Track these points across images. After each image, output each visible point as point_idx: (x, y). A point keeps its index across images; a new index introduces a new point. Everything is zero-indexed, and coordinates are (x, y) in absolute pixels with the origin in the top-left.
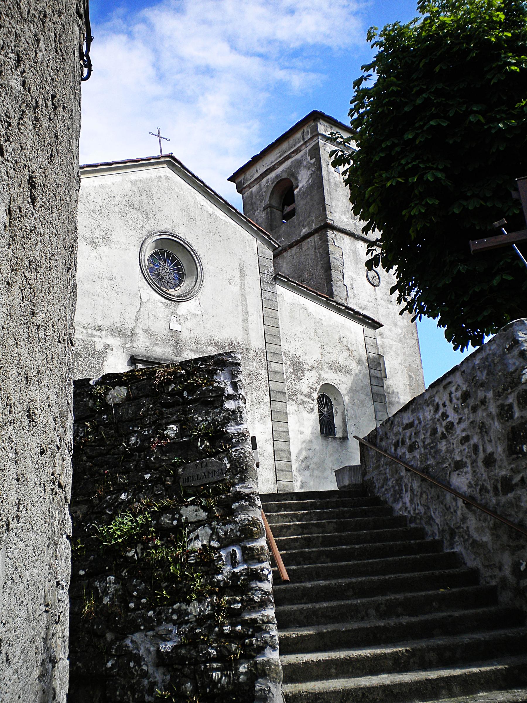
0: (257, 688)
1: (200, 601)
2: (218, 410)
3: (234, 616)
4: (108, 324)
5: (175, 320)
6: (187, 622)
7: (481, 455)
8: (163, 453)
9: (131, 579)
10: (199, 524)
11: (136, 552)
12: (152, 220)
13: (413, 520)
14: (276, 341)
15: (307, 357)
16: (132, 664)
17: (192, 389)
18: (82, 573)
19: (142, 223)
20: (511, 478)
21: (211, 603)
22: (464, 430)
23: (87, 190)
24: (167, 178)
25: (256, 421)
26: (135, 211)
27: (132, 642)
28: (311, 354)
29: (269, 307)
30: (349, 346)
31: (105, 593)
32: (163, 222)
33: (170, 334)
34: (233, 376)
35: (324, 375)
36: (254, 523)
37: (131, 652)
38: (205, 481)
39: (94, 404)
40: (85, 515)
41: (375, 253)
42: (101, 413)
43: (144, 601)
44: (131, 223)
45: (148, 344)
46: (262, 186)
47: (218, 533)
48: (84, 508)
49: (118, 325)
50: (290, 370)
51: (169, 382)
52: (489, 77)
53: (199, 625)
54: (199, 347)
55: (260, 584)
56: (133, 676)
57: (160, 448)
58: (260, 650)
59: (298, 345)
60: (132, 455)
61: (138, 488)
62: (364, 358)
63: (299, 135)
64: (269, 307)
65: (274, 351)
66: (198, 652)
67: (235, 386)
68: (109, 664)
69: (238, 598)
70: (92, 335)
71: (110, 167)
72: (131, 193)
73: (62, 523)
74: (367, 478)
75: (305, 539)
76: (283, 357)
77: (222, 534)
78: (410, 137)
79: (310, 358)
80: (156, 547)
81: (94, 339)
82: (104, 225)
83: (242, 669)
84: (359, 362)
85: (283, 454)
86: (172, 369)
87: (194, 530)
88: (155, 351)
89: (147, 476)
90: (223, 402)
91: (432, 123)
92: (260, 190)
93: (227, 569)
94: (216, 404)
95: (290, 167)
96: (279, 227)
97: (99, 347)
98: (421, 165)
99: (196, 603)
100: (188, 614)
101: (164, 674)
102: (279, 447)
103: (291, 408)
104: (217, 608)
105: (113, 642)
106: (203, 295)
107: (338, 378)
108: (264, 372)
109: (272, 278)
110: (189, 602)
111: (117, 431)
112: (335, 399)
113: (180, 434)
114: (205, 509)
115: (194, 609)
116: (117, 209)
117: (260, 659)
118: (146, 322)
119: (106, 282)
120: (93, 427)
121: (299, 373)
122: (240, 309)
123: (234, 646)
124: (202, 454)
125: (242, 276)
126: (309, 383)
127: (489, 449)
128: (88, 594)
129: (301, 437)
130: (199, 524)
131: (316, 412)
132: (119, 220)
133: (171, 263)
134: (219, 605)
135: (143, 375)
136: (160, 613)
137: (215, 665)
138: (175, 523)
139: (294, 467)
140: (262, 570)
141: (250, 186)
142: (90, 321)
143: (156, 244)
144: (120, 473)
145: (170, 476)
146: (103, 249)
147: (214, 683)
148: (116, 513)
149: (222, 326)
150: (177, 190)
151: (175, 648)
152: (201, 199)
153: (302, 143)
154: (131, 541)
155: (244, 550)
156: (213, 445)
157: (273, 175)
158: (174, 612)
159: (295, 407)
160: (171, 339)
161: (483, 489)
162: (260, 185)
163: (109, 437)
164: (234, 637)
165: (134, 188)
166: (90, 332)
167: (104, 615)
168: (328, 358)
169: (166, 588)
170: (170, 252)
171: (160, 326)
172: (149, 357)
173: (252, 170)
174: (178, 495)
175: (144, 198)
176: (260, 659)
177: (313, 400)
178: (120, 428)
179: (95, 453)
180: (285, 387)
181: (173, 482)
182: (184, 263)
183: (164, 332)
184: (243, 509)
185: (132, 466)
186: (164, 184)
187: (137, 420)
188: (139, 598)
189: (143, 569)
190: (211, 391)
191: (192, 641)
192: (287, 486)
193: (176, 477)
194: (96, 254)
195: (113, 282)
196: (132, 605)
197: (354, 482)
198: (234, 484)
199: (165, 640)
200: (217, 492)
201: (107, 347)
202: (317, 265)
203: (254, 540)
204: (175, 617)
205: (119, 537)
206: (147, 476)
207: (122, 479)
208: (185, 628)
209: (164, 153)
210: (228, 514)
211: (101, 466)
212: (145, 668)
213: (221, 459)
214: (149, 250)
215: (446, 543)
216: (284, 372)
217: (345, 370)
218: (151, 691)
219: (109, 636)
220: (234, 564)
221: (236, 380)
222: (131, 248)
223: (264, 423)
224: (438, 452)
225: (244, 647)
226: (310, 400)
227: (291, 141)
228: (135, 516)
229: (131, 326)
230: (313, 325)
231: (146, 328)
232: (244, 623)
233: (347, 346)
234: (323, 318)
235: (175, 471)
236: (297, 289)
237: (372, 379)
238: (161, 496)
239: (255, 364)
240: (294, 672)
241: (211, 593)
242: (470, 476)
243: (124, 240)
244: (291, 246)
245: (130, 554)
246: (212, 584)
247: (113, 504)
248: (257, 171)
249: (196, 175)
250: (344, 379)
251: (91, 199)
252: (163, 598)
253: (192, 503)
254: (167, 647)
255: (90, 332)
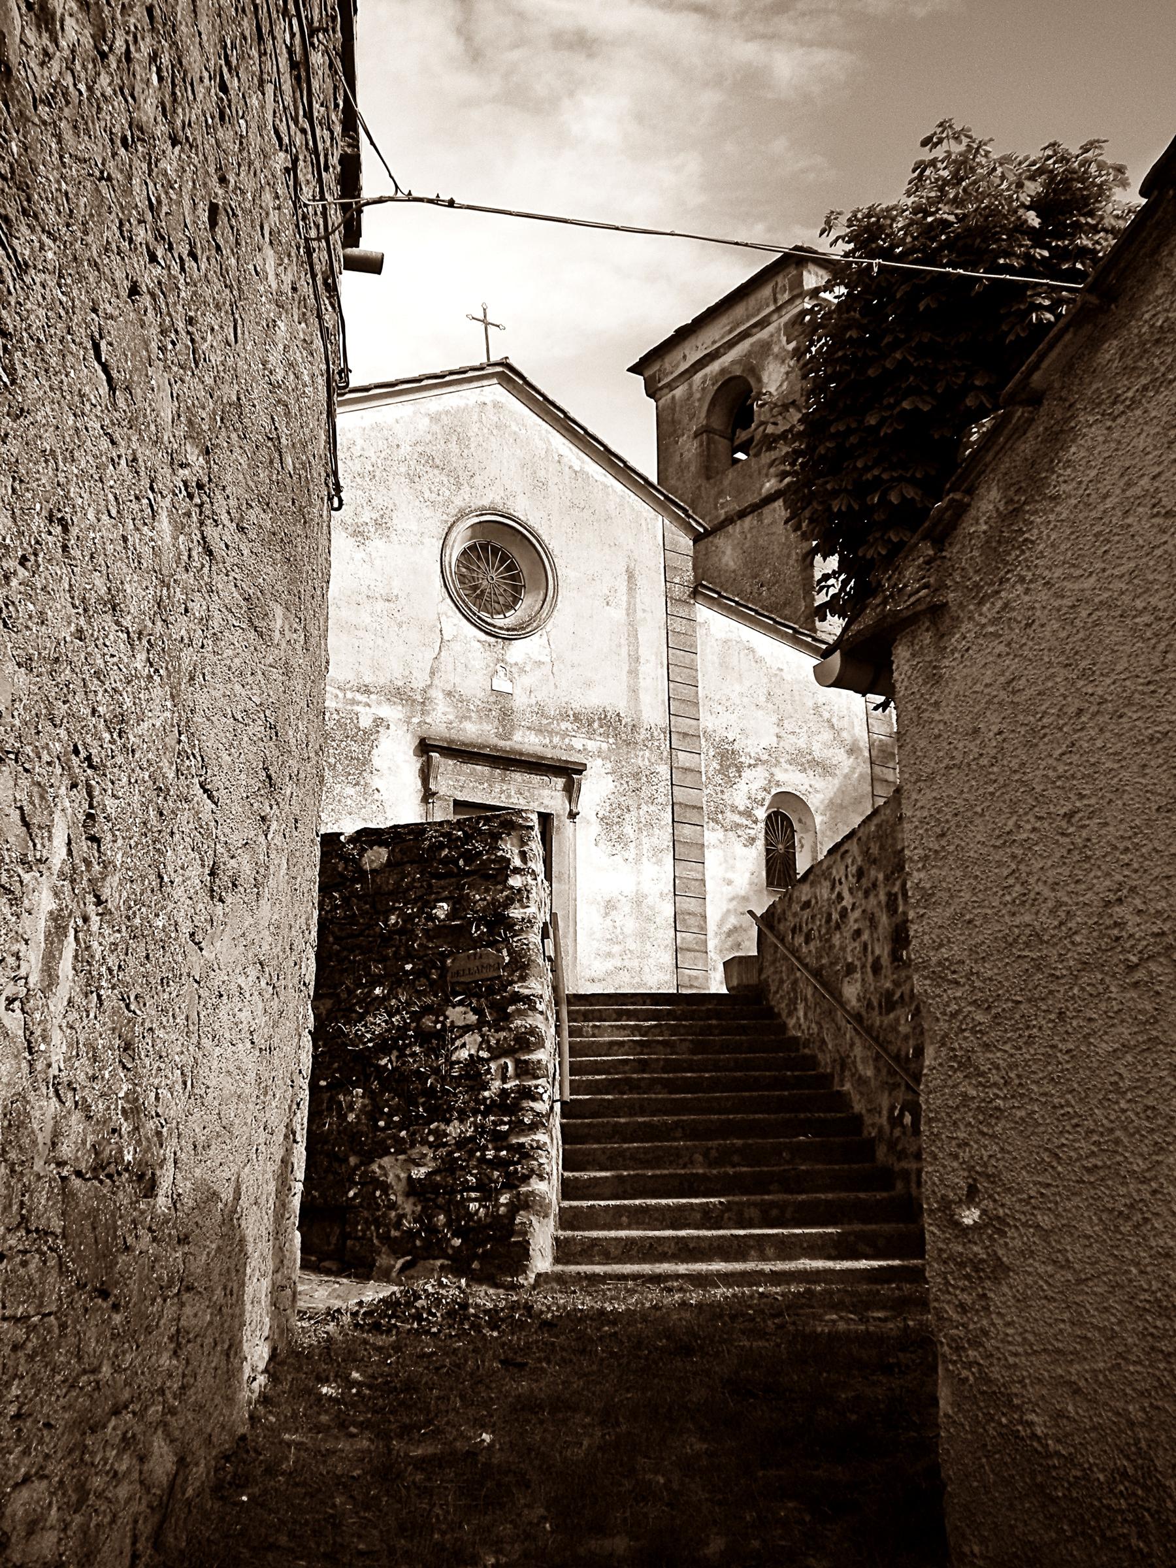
0: (517, 1221)
1: (462, 1121)
2: (500, 887)
3: (499, 1139)
4: (382, 681)
5: (501, 673)
6: (445, 1145)
7: (870, 959)
8: (430, 939)
9: (382, 1093)
10: (467, 1029)
11: (390, 1061)
12: (466, 488)
13: (807, 1044)
14: (691, 711)
15: (749, 742)
16: (378, 1193)
17: (470, 857)
18: (323, 1083)
19: (447, 493)
20: (893, 993)
21: (474, 1123)
22: (856, 921)
23: (349, 435)
24: (497, 405)
25: (644, 859)
26: (436, 472)
27: (380, 1167)
28: (756, 734)
29: (680, 646)
30: (834, 720)
31: (351, 1108)
32: (486, 491)
33: (492, 699)
34: (523, 843)
35: (780, 776)
36: (533, 1031)
37: (377, 1179)
38: (478, 976)
39: (345, 869)
40: (329, 1012)
41: (832, 591)
42: (355, 881)
43: (396, 1119)
44: (427, 494)
45: (451, 717)
46: (695, 387)
47: (488, 1042)
48: (329, 1003)
49: (400, 684)
50: (715, 765)
51: (442, 846)
52: (1005, 328)
53: (459, 1150)
54: (545, 722)
55: (532, 1104)
56: (378, 1208)
57: (426, 932)
58: (525, 1179)
59: (733, 718)
60: (390, 938)
61: (396, 981)
62: (864, 743)
63: (766, 292)
64: (680, 646)
65: (685, 730)
66: (455, 1179)
67: (523, 855)
68: (351, 1194)
69: (506, 1119)
70: (354, 702)
71: (392, 389)
72: (429, 437)
73: (305, 1017)
74: (763, 977)
75: (640, 1060)
76: (703, 741)
77: (493, 1042)
78: (873, 422)
79: (751, 746)
80: (414, 1054)
81: (356, 708)
82: (379, 501)
83: (503, 1199)
84: (852, 751)
85: (691, 921)
86: (446, 828)
87: (461, 1036)
88: (464, 730)
89: (408, 967)
90: (508, 876)
91: (906, 405)
92: (690, 395)
93: (496, 1084)
94: (499, 878)
95: (749, 355)
96: (723, 472)
97: (365, 722)
98: (885, 476)
99: (456, 1123)
100: (446, 1135)
101: (415, 1205)
102: (685, 906)
103: (712, 836)
104: (480, 1129)
105: (357, 1167)
106: (555, 626)
107: (807, 782)
108: (664, 770)
109: (688, 591)
110: (448, 1122)
111: (373, 906)
112: (800, 821)
113: (451, 916)
114: (475, 1011)
115: (454, 1129)
116: (403, 469)
117: (523, 1189)
118: (449, 677)
119: (380, 605)
120: (343, 898)
121: (732, 772)
122: (624, 651)
123: (496, 1173)
124: (476, 943)
125: (630, 589)
126: (750, 790)
127: (877, 952)
128: (330, 1109)
129: (729, 891)
130: (467, 1029)
131: (760, 844)
132: (406, 490)
133: (499, 567)
134: (483, 1126)
135: (409, 834)
136: (414, 1133)
137: (473, 1195)
138: (439, 1026)
139: (711, 945)
140: (536, 1087)
141: (670, 386)
142: (351, 676)
143: (474, 532)
144: (375, 961)
145: (437, 968)
146: (377, 544)
147: (470, 1216)
148: (367, 1012)
149: (589, 684)
150: (514, 428)
151: (428, 1174)
152: (560, 443)
153: (772, 308)
154: (384, 1045)
155: (518, 1063)
156: (491, 932)
157: (715, 367)
158: (431, 1132)
159: (720, 834)
160: (494, 707)
161: (869, 1006)
162: (690, 386)
163: (363, 913)
164: (498, 1163)
165: (436, 428)
166: (349, 695)
167: (350, 1135)
168: (789, 743)
169: (423, 1104)
170: (498, 545)
171: (474, 685)
172: (452, 741)
173: (676, 355)
174: (444, 992)
175: (453, 447)
176: (523, 1189)
177: (755, 822)
178: (378, 901)
179: (344, 934)
180: (703, 798)
181: (440, 976)
182: (524, 565)
183: (481, 695)
184: (520, 1013)
185: (390, 952)
186: (491, 416)
187: (398, 893)
188: (390, 1115)
189: (398, 1081)
190: (493, 861)
191: (449, 1166)
192: (696, 978)
193: (444, 969)
194: (363, 555)
195: (392, 605)
196: (381, 1123)
197: (745, 981)
198: (511, 983)
199: (418, 1165)
200: (491, 991)
201: (379, 722)
202: (789, 556)
203: (531, 1051)
204: (431, 1139)
205: (370, 1040)
206: (408, 967)
207: (376, 969)
208: (443, 1151)
209: (493, 359)
210: (502, 1018)
211: (351, 951)
212: (393, 1197)
213: (499, 951)
214: (459, 542)
215: (836, 1079)
216: (703, 770)
217: (824, 768)
218: (398, 1225)
219: (353, 1160)
220: (504, 1079)
221: (526, 849)
222: (426, 540)
223: (659, 862)
224: (832, 947)
225: (508, 1175)
226: (749, 823)
227: (752, 301)
228: (391, 1015)
229: (422, 685)
230: (765, 680)
231: (449, 688)
232: (511, 1148)
233: (829, 721)
234: (785, 667)
235: (444, 962)
236: (735, 612)
237: (876, 784)
238: (425, 993)
239: (647, 753)
240: (575, 1216)
241: (475, 1112)
242: (858, 985)
243: (414, 528)
244: (742, 515)
245: (383, 1062)
246: (477, 1102)
247: (364, 1000)
248: (685, 357)
249: (551, 397)
250: (819, 783)
251: (356, 451)
252: (418, 1116)
253: (461, 1003)
254: (419, 1173)
255: (349, 695)
